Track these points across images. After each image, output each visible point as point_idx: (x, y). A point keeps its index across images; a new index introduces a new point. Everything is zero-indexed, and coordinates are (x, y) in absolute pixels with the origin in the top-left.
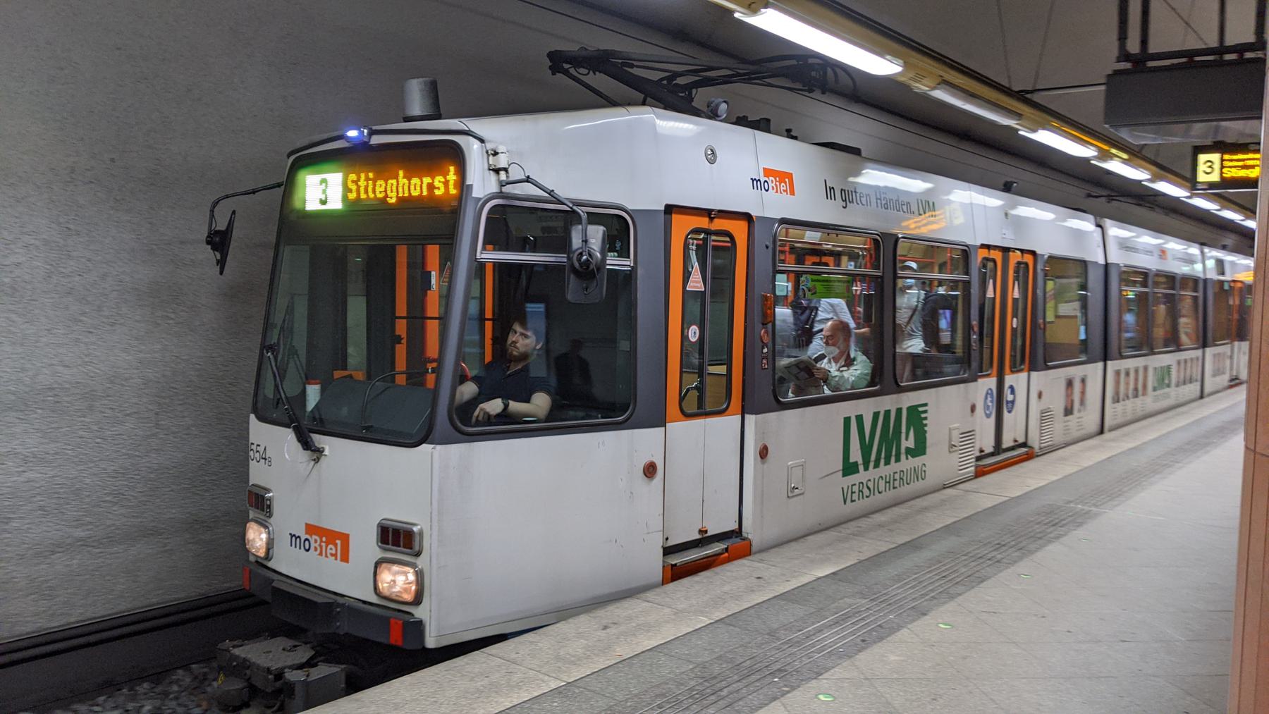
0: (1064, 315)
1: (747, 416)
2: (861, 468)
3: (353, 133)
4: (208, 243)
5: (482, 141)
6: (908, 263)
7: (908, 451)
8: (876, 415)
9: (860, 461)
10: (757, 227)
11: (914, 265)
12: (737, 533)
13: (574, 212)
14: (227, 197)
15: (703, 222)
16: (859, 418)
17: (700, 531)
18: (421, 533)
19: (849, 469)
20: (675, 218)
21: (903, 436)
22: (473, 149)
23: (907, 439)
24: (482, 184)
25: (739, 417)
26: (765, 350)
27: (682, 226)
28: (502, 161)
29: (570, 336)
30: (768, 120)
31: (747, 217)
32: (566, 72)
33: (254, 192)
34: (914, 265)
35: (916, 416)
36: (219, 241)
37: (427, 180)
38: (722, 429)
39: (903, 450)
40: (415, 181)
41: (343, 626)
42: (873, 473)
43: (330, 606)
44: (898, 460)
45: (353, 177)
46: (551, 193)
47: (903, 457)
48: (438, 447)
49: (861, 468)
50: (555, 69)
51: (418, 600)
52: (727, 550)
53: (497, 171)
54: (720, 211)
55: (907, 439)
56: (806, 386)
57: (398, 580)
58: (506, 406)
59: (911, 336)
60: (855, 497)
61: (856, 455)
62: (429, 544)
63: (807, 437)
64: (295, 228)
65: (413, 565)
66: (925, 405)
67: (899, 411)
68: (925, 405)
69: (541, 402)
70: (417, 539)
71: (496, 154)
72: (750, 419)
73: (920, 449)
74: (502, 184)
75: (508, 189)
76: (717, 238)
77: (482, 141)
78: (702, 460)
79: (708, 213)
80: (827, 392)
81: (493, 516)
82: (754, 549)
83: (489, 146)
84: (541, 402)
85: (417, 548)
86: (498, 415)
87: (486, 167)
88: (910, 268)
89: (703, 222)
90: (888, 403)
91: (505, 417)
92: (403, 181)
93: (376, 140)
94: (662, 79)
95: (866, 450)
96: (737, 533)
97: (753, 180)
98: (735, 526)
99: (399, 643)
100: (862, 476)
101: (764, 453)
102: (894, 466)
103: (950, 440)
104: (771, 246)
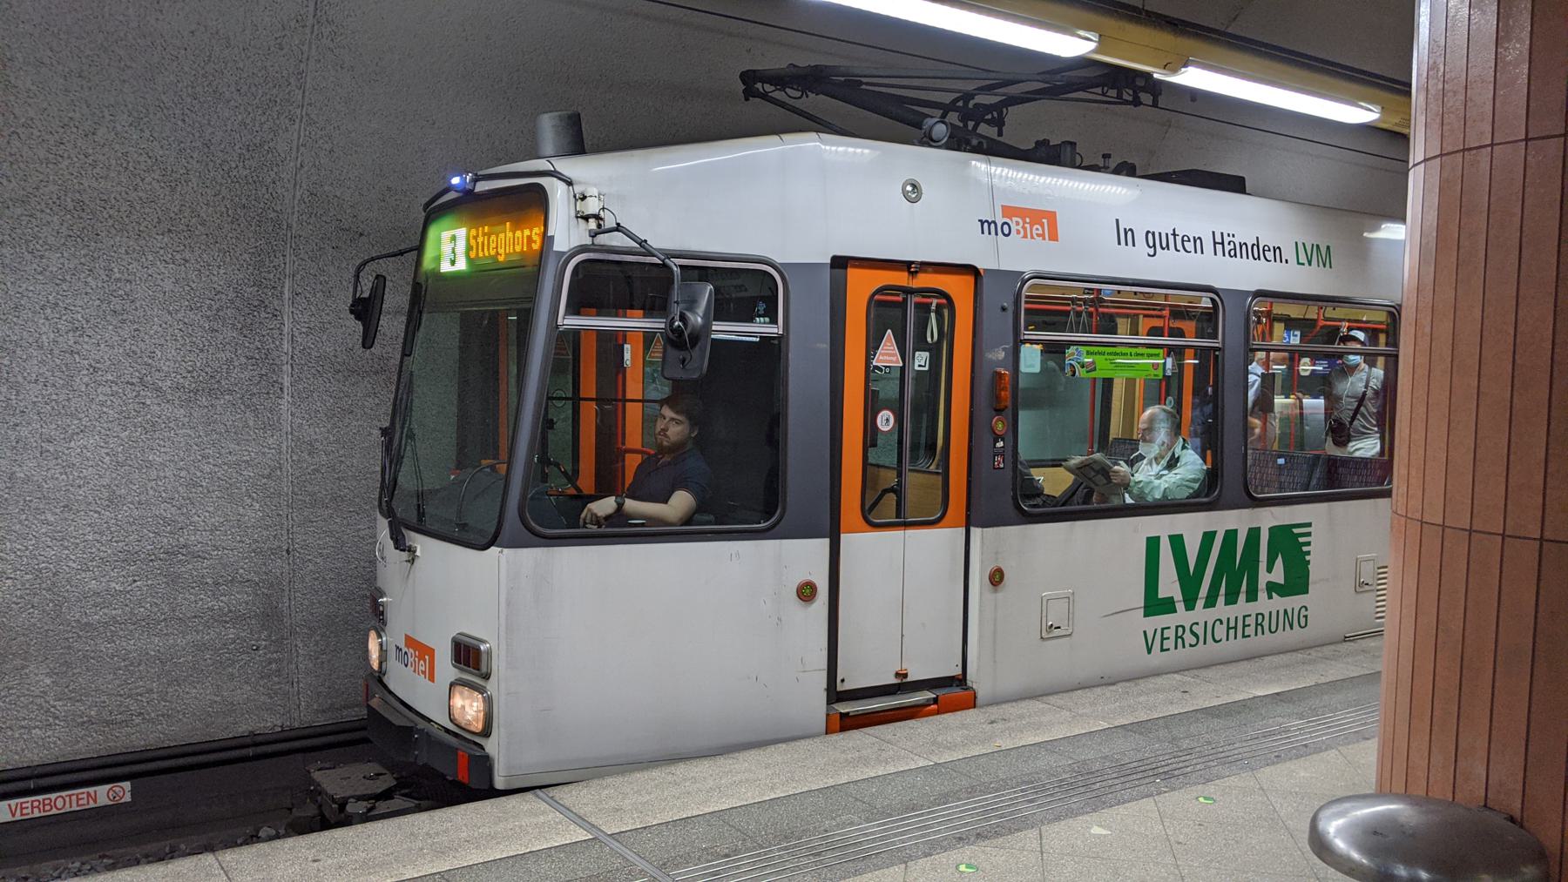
0: (842, 383)
1: (973, 529)
2: (1180, 606)
3: (456, 181)
4: (352, 312)
5: (570, 183)
6: (1353, 333)
7: (1272, 588)
8: (1209, 537)
9: (1178, 596)
10: (986, 281)
11: (1361, 335)
12: (960, 681)
13: (664, 265)
14: (373, 259)
15: (900, 279)
16: (1177, 542)
17: (897, 675)
18: (489, 652)
19: (1155, 605)
20: (853, 274)
21: (1263, 565)
22: (558, 193)
23: (1269, 570)
24: (566, 233)
25: (963, 530)
26: (1000, 444)
27: (861, 286)
28: (592, 206)
29: (714, 419)
30: (1073, 144)
31: (971, 270)
32: (765, 96)
33: (401, 253)
34: (1361, 335)
35: (1289, 544)
36: (365, 310)
37: (527, 232)
38: (933, 546)
39: (1262, 585)
40: (518, 233)
41: (422, 756)
42: (1200, 614)
43: (409, 731)
44: (1252, 596)
45: (473, 232)
46: (642, 243)
47: (1263, 595)
48: (506, 551)
49: (1180, 606)
50: (749, 93)
51: (486, 732)
52: (935, 701)
53: (586, 218)
54: (923, 264)
55: (1269, 570)
56: (1094, 498)
57: (469, 708)
58: (620, 506)
59: (1362, 435)
60: (1169, 644)
61: (1169, 585)
62: (499, 665)
63: (1092, 563)
64: (427, 293)
65: (481, 690)
66: (1309, 525)
67: (1254, 534)
68: (1309, 525)
69: (681, 502)
70: (484, 658)
71: (584, 198)
72: (976, 532)
73: (1297, 582)
74: (594, 235)
75: (603, 239)
76: (909, 299)
77: (570, 183)
78: (905, 583)
79: (906, 266)
80: (1129, 500)
81: (603, 634)
82: (979, 702)
83: (578, 189)
84: (681, 502)
85: (484, 669)
86: (607, 518)
87: (573, 213)
88: (1355, 339)
89: (900, 279)
90: (1236, 520)
91: (619, 516)
92: (510, 234)
93: (482, 187)
94: (957, 100)
95: (1190, 584)
96: (960, 681)
97: (982, 222)
98: (958, 671)
99: (465, 781)
100: (1182, 616)
101: (996, 578)
102: (1242, 607)
103: (1358, 574)
104: (1011, 309)
